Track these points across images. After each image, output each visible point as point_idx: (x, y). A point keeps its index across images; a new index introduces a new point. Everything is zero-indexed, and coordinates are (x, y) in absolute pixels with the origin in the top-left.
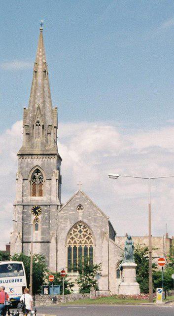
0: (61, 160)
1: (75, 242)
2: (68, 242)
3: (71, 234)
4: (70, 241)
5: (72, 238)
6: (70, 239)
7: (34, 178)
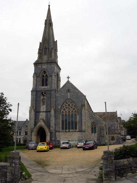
0: (61, 69)
1: (66, 112)
2: (62, 111)
3: (64, 107)
4: (63, 111)
5: (64, 109)
6: (63, 110)
7: (43, 76)
